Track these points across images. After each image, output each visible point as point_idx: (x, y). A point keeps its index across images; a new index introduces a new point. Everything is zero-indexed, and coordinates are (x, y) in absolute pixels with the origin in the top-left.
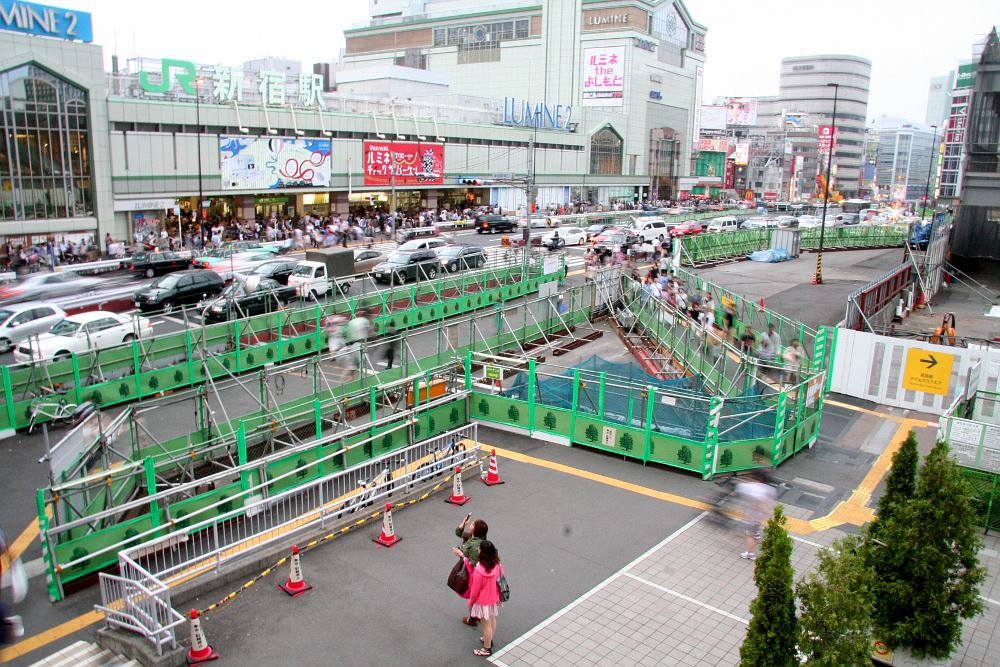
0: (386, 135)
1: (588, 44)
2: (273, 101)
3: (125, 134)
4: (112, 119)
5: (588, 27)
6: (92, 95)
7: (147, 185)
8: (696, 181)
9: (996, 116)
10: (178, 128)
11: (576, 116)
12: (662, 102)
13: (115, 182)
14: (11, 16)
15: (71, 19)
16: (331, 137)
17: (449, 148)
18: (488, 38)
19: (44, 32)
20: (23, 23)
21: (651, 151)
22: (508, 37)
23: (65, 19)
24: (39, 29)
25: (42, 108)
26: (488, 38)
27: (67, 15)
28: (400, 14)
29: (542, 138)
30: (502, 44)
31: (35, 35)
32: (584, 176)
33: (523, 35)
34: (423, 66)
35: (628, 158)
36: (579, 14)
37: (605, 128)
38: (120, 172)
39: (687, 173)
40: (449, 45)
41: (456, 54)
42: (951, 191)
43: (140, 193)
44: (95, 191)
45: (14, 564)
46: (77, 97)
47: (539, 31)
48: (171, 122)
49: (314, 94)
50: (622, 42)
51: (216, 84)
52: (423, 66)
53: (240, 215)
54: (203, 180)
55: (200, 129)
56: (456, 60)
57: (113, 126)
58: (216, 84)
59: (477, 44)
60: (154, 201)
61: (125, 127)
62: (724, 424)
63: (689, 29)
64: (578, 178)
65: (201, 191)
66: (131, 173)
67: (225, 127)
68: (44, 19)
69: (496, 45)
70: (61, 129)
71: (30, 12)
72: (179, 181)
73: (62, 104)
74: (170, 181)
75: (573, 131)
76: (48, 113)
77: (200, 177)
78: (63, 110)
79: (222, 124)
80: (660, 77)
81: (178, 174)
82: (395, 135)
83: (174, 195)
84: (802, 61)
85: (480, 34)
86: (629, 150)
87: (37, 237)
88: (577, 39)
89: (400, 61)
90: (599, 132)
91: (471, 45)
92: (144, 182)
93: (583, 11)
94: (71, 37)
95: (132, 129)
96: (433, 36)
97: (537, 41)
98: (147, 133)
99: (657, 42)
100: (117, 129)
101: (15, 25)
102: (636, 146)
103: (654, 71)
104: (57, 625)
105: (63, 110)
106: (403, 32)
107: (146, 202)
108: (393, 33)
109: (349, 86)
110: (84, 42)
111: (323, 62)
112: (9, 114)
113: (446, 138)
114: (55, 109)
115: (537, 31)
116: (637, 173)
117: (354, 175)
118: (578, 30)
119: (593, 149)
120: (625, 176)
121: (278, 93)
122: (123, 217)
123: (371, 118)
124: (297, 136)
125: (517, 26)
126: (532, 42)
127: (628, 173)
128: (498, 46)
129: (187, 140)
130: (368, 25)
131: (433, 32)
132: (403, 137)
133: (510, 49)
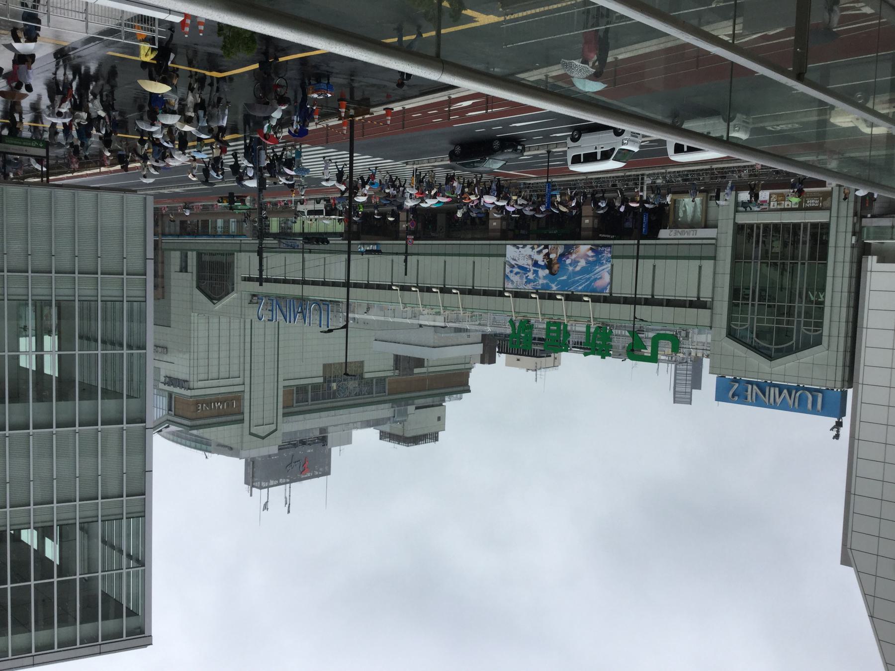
0: (411, 290)
1: (237, 381)
3: (698, 298)
4: (708, 312)
5: (237, 398)
6: (724, 332)
7: (684, 251)
9: (384, 411)
10: (368, 286)
11: (251, 312)
13: (713, 255)
14: (782, 396)
15: (733, 396)
16: (504, 291)
19: (758, 384)
20: (774, 391)
21: (163, 277)
22: (315, 387)
23: (738, 395)
24: (762, 387)
25: (769, 321)
26: (334, 386)
27: (736, 398)
28: (417, 408)
29: (295, 290)
30: (321, 380)
31: (766, 382)
32: (240, 251)
33: (302, 390)
34: (397, 358)
35: (189, 269)
36: (246, 410)
37: (219, 299)
38: (708, 265)
40: (372, 379)
41: (365, 370)
45: (65, 102)
48: (654, 307)
50: (201, 384)
52: (397, 358)
53: (504, 223)
55: (634, 301)
56: (366, 364)
60: (679, 236)
61: (698, 304)
62: (151, 25)
64: (247, 249)
66: (442, 258)
68: (765, 395)
69: (327, 380)
71: (767, 401)
72: (675, 254)
74: (683, 255)
75: (254, 295)
77: (406, 254)
78: (752, 319)
79: (485, 298)
81: (653, 261)
83: (658, 242)
89: (420, 362)
93: (243, 413)
94: (735, 380)
96: (387, 387)
97: (287, 383)
98: (677, 298)
99: (161, 386)
101: (781, 388)
103: (165, 358)
105: (752, 319)
106: (420, 391)
107: (686, 236)
108: (428, 390)
109: (470, 340)
110: (725, 377)
111: (486, 366)
115: (288, 391)
116: (178, 254)
118: (247, 396)
120: (192, 250)
122: (710, 223)
123: (464, 309)
124: (537, 293)
125: (307, 398)
126: (292, 383)
127: (189, 253)
129: (644, 292)
131: (387, 391)
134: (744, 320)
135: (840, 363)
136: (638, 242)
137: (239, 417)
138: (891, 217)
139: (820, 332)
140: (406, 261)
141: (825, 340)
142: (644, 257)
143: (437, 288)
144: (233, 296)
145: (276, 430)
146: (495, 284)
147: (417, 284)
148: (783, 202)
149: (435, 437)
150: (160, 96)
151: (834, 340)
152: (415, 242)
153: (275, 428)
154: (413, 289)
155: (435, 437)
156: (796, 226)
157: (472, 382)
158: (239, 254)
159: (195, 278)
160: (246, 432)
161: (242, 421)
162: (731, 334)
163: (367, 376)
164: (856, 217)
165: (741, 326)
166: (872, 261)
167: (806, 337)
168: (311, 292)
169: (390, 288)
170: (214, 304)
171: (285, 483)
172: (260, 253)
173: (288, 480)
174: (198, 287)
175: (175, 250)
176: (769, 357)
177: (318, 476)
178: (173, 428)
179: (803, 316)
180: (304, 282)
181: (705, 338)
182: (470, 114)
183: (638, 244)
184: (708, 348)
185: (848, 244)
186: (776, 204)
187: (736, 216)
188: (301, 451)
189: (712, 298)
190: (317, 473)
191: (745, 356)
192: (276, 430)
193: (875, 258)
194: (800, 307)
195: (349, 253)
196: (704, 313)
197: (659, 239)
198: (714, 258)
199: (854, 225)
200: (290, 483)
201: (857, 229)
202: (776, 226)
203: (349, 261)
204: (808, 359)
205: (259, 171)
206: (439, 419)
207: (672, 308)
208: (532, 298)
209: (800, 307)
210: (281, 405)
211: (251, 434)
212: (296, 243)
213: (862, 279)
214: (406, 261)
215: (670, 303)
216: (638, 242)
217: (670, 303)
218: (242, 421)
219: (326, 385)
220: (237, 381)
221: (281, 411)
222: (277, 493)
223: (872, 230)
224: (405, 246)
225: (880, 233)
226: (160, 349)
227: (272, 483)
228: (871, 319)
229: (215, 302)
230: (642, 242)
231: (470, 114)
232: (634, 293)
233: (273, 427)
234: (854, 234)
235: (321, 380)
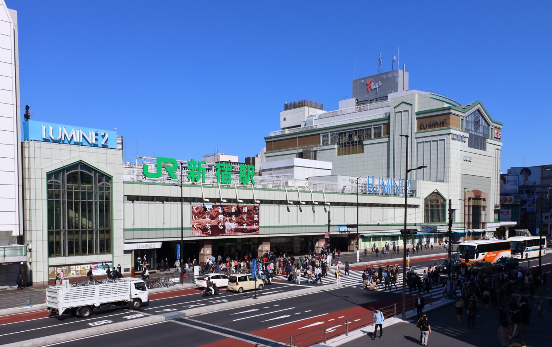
1: (420, 140)
3: (358, 208)
7: (145, 234)
8: (499, 225)
17: (263, 209)
18: (356, 139)
21: (465, 206)
22: (369, 137)
28: (300, 126)
29: (363, 199)
30: (365, 142)
37: (434, 192)
39: (492, 220)
42: (324, 136)
44: (113, 238)
46: (442, 200)
57: (126, 197)
59: (348, 143)
65: (182, 237)
77: (182, 229)
78: (96, 189)
82: (299, 202)
85: (350, 136)
87: (74, 267)
89: (301, 156)
91: (345, 143)
92: (158, 232)
104: (391, 326)
113: (331, 203)
119: (426, 206)
128: (363, 145)
132: (225, 201)
136: (182, 239)
138: (7, 263)
139: (49, 181)
140: (329, 221)
141: (45, 176)
142: (177, 229)
145: (395, 108)
148: (81, 269)
150: (22, 263)
152: (324, 234)
153: (395, 109)
156: (71, 253)
158: (421, 222)
162: (109, 178)
164: (30, 261)
167: (56, 178)
168: (353, 199)
170: (436, 190)
176: (81, 164)
180: (358, 205)
182: (288, 316)
183: (182, 237)
184: (124, 168)
186: (86, 268)
187: (112, 259)
191: (99, 164)
192: (395, 108)
195: (329, 226)
197: (161, 242)
198: (125, 230)
201: (28, 254)
202: (84, 252)
205: (451, 277)
207: (134, 195)
211: (411, 105)
212: (424, 230)
213: (108, 217)
214: (329, 221)
216: (182, 239)
218: (417, 114)
220: (420, 140)
224: (330, 231)
226: (468, 159)
229: (436, 191)
230: (180, 239)
231: (288, 316)
232: (183, 205)
233: (397, 110)
234: (30, 250)
235: (365, 142)
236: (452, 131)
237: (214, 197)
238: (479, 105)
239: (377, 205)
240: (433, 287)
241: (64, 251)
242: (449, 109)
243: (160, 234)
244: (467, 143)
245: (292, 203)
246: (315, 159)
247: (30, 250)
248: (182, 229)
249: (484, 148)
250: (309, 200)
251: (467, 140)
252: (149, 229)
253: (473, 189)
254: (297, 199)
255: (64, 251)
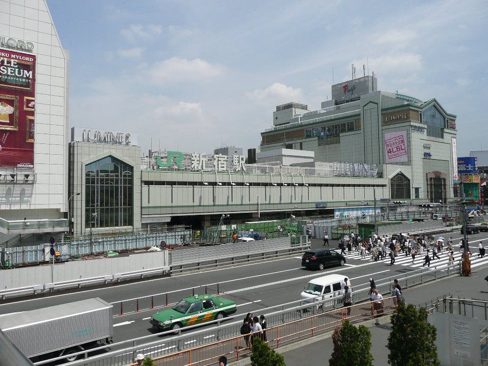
0: (298, 184)
2: (220, 169)
12: (431, 158)
21: (427, 185)
22: (343, 131)
30: (341, 135)
33: (351, 129)
37: (398, 174)
38: (145, 204)
43: (149, 217)
47: (360, 126)
49: (240, 164)
51: (193, 162)
54: (143, 209)
58: (193, 162)
63: (444, 118)
67: (176, 182)
70: (119, 185)
73: (121, 173)
76: (114, 178)
78: (121, 176)
80: (430, 145)
83: (171, 215)
84: (438, 104)
86: (414, 184)
88: (380, 128)
90: (394, 177)
92: (162, 209)
95: (152, 184)
97: (359, 132)
100: (145, 184)
102: (418, 181)
105: (121, 176)
111: (252, 148)
112: (98, 179)
114: (117, 176)
117: (261, 204)
118: (380, 124)
121: (222, 165)
125: (348, 125)
126: (357, 132)
128: (339, 136)
130: (273, 129)
133: (345, 137)
134: (125, 176)
135: (76, 156)
137: (384, 112)
143: (219, 185)
144: (391, 177)
146: (253, 189)
147: (232, 187)
149: (278, 108)
151: (80, 167)
154: (234, 184)
155: (278, 108)
157: (260, 139)
159: (411, 185)
160: (380, 105)
161: (382, 110)
162: (131, 168)
163: (317, 138)
165: (126, 173)
166: (64, 209)
169: (309, 185)
171: (355, 80)
172: (375, 200)
173: (354, 81)
174: (409, 180)
175: (422, 199)
177: (338, 85)
178: (419, 105)
179: (99, 183)
181: (143, 167)
185: (75, 217)
188: (348, 96)
189: (141, 187)
190: (339, 86)
192: (364, 106)
193: (62, 211)
194: (97, 186)
196: (145, 179)
199: (73, 228)
200: (353, 80)
203: (375, 199)
204: (92, 157)
206: (277, 118)
208: (235, 183)
209: (97, 186)
210: (362, 119)
215: (184, 183)
217: (184, 183)
218: (382, 110)
219: (338, 132)
221: (362, 115)
222: (359, 76)
223: (64, 226)
225: (59, 224)
227: (363, 80)
228: (63, 180)
233: (365, 108)
235: (341, 135)
236: (412, 124)
237: (212, 181)
238: (434, 102)
239: (359, 185)
240: (398, 255)
241: (121, 222)
242: (408, 105)
243: (169, 210)
244: (425, 133)
245: (221, 184)
246: (301, 149)
247: (411, 203)
248: (375, 200)
249: (442, 137)
250: (226, 181)
251: (425, 130)
252: (161, 207)
253: (434, 171)
254: (301, 182)
255: (121, 222)
